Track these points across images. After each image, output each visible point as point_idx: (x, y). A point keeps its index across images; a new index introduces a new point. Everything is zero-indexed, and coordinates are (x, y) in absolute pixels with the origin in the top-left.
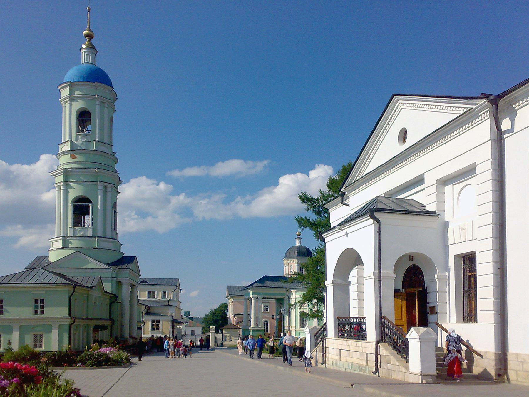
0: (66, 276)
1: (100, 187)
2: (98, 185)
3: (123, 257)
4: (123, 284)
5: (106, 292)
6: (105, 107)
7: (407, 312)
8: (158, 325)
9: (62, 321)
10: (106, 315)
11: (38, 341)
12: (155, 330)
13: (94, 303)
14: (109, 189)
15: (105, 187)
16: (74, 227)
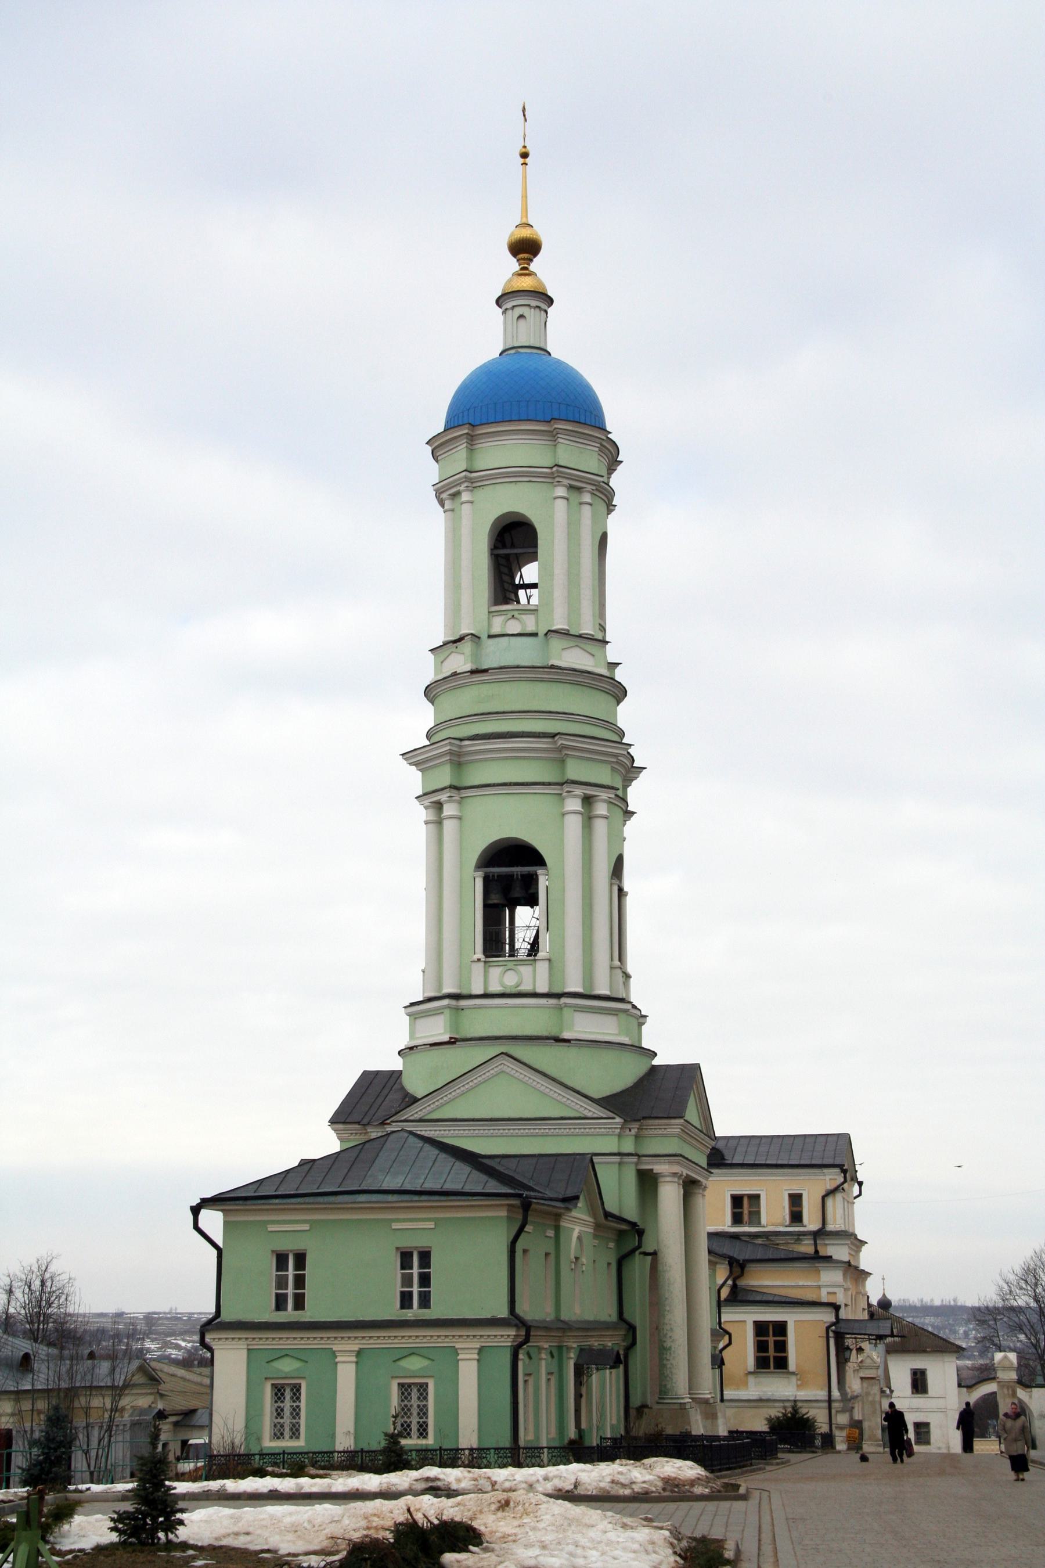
0: (480, 1159)
1: (574, 804)
2: (564, 794)
3: (654, 1068)
4: (662, 1179)
5: (607, 1215)
6: (581, 503)
7: (215, 1479)
8: (782, 1346)
9: (254, 1339)
10: (608, 1312)
11: (415, 1411)
12: (769, 1368)
13: (577, 1258)
14: (601, 809)
15: (588, 801)
16: (488, 959)
